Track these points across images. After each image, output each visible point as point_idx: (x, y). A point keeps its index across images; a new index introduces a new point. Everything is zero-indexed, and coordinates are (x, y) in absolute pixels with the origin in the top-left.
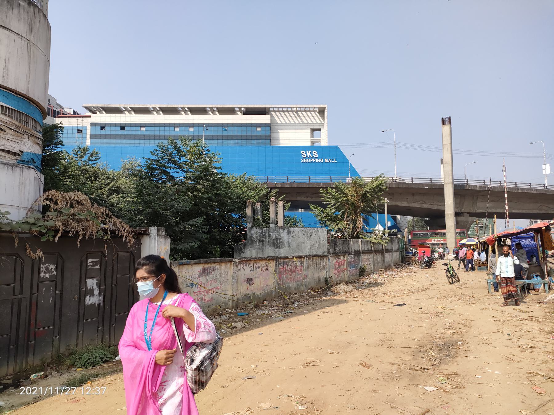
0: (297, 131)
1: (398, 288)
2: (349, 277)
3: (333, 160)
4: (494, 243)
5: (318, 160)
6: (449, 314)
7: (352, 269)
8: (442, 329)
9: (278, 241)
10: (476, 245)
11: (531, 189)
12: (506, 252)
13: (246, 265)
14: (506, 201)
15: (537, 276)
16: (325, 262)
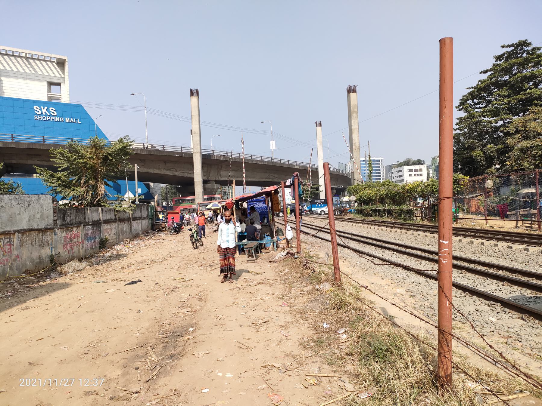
1: (141, 259)
2: (85, 251)
3: (76, 120)
4: (233, 206)
5: (56, 119)
6: (187, 286)
7: (89, 242)
8: (176, 309)
10: (220, 209)
11: (262, 161)
12: (227, 218)
14: (244, 170)
15: (267, 236)
16: (49, 236)
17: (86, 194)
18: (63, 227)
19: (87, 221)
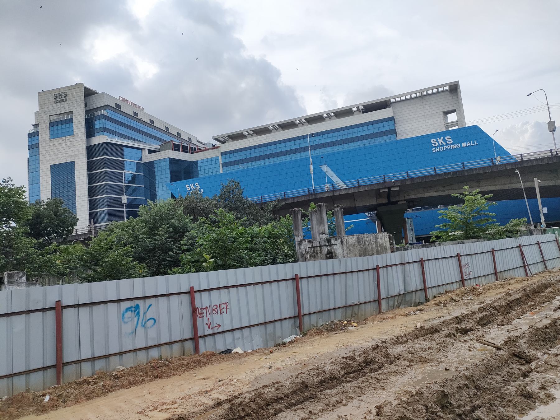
3: (473, 143)
5: (453, 146)
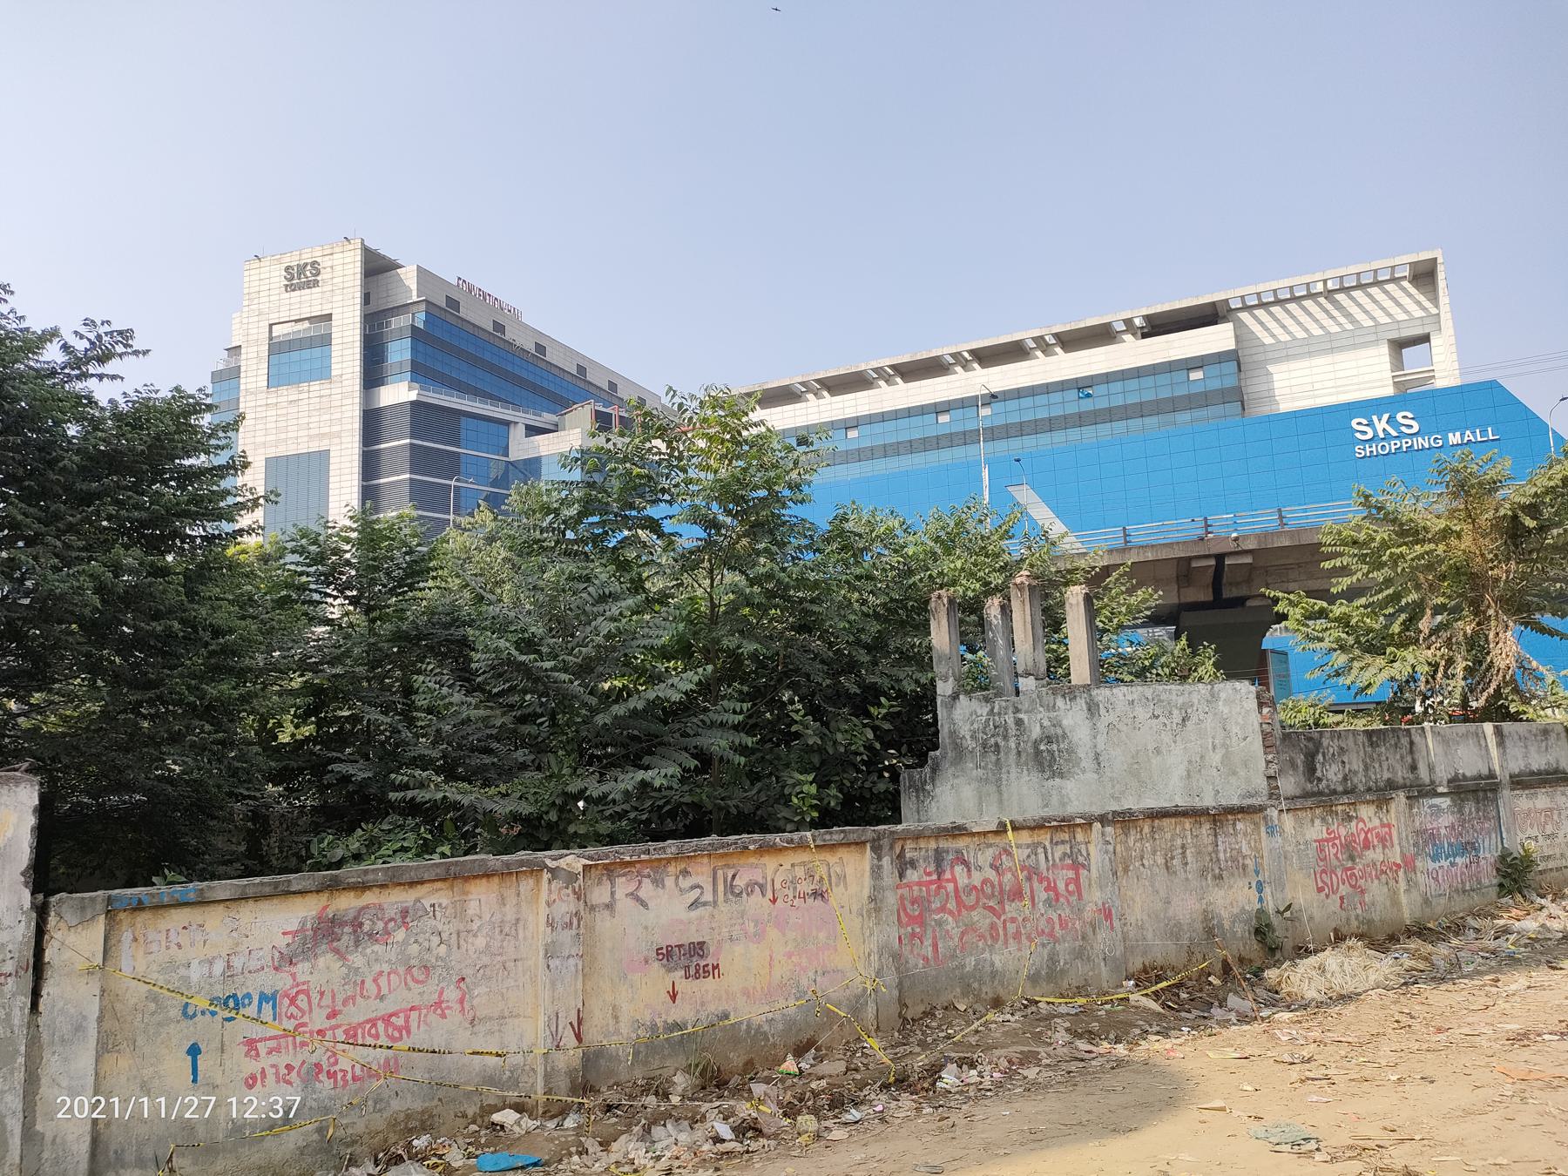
0: (1339, 357)
2: (1427, 902)
5: (1420, 442)
9: (1055, 747)
13: (659, 883)
16: (1242, 837)
17: (1445, 672)
18: (1309, 803)
19: (1427, 781)
